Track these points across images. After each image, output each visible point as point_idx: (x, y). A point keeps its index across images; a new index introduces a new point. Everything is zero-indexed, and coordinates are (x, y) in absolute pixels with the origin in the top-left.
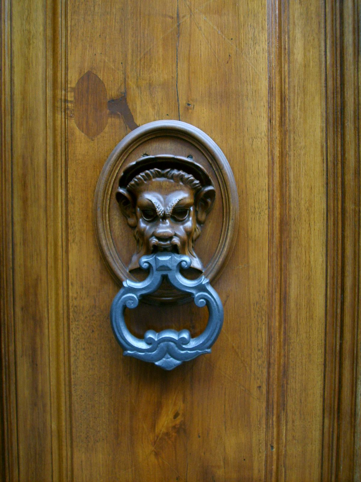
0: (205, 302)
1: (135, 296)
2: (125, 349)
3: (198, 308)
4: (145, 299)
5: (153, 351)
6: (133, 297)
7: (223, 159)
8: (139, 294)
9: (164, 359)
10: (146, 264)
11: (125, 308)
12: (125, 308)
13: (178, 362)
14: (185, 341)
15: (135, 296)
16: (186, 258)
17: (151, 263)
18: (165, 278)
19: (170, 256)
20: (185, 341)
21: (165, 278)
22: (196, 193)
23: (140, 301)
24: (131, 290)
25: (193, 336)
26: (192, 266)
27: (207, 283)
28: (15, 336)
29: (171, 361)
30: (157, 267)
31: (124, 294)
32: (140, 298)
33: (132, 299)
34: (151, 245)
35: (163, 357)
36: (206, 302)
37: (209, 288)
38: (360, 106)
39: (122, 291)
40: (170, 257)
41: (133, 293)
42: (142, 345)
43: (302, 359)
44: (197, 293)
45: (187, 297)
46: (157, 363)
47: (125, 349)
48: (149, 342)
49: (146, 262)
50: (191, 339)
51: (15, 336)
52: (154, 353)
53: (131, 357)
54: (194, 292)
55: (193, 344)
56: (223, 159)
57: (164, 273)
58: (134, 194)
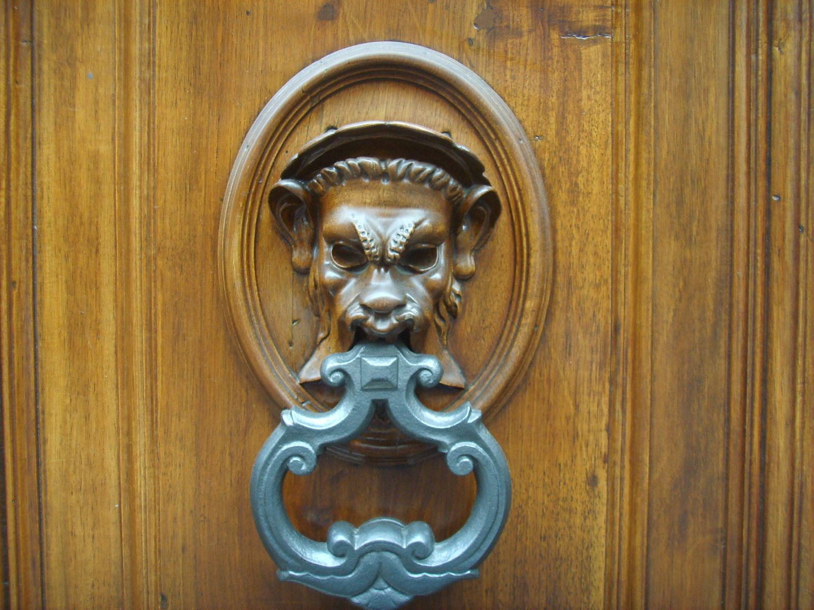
0: (471, 463)
1: (310, 448)
2: (281, 565)
3: (455, 477)
4: (330, 453)
5: (350, 573)
6: (306, 450)
7: (502, 114)
8: (319, 442)
9: (374, 591)
10: (338, 375)
11: (284, 471)
12: (284, 471)
13: (403, 598)
14: (421, 552)
15: (310, 448)
16: (431, 363)
17: (349, 372)
18: (380, 410)
19: (392, 356)
20: (421, 552)
21: (380, 410)
22: (456, 214)
23: (319, 457)
24: (298, 432)
25: (443, 534)
26: (441, 382)
27: (478, 422)
28: (37, 433)
29: (387, 596)
30: (364, 384)
31: (284, 440)
32: (320, 453)
33: (303, 457)
34: (349, 323)
35: (371, 585)
36: (474, 465)
37: (484, 434)
38: (812, 43)
39: (279, 433)
40: (394, 359)
41: (308, 442)
42: (323, 558)
43: (549, 123)
44: (453, 444)
45: (430, 452)
46: (356, 600)
47: (281, 565)
48: (339, 551)
49: (339, 370)
50: (438, 546)
51: (37, 433)
52: (350, 576)
53: (292, 584)
54: (445, 440)
55: (444, 554)
56: (502, 114)
57: (380, 396)
58: (315, 208)
